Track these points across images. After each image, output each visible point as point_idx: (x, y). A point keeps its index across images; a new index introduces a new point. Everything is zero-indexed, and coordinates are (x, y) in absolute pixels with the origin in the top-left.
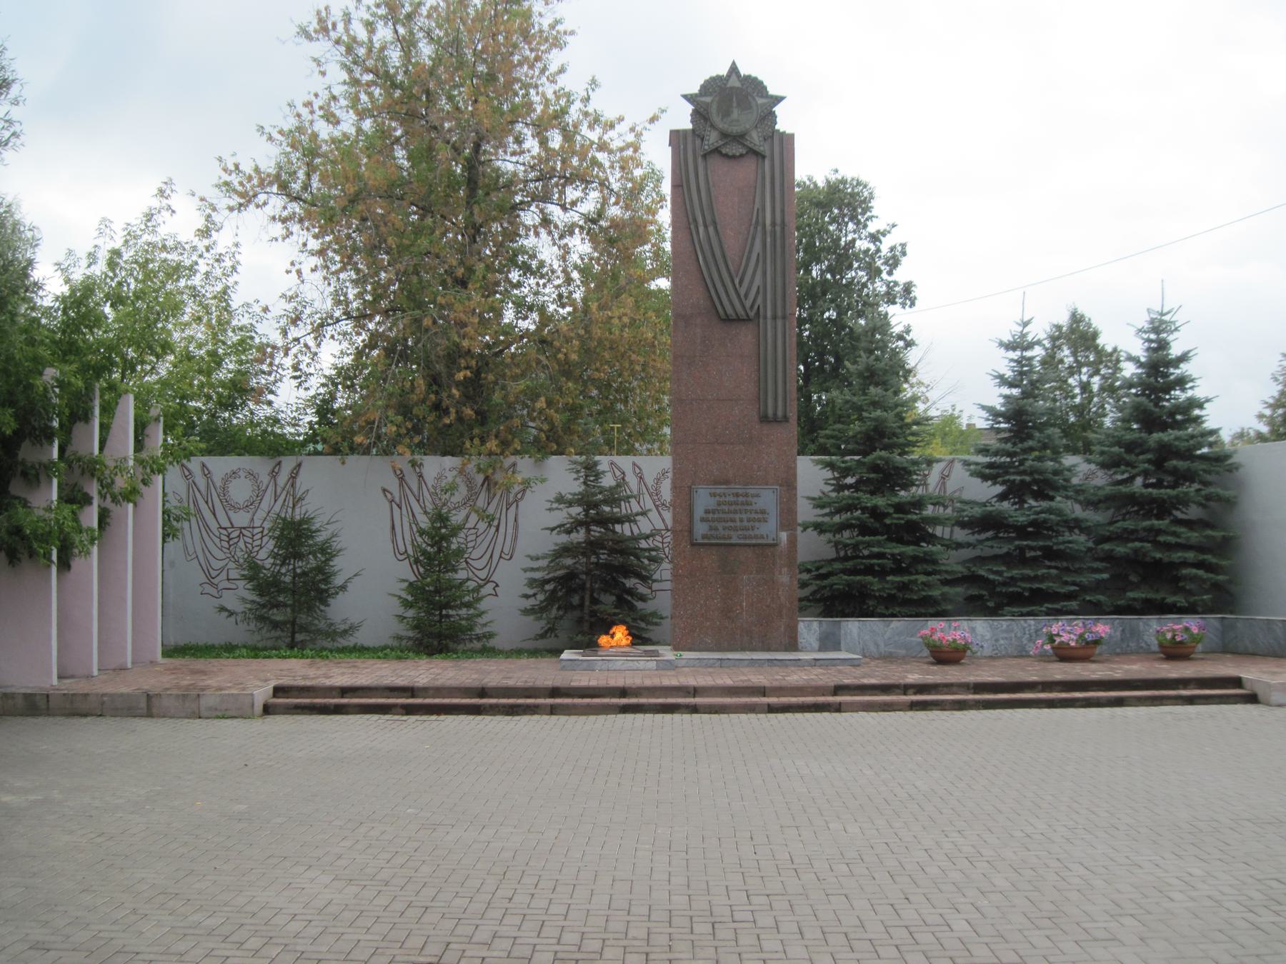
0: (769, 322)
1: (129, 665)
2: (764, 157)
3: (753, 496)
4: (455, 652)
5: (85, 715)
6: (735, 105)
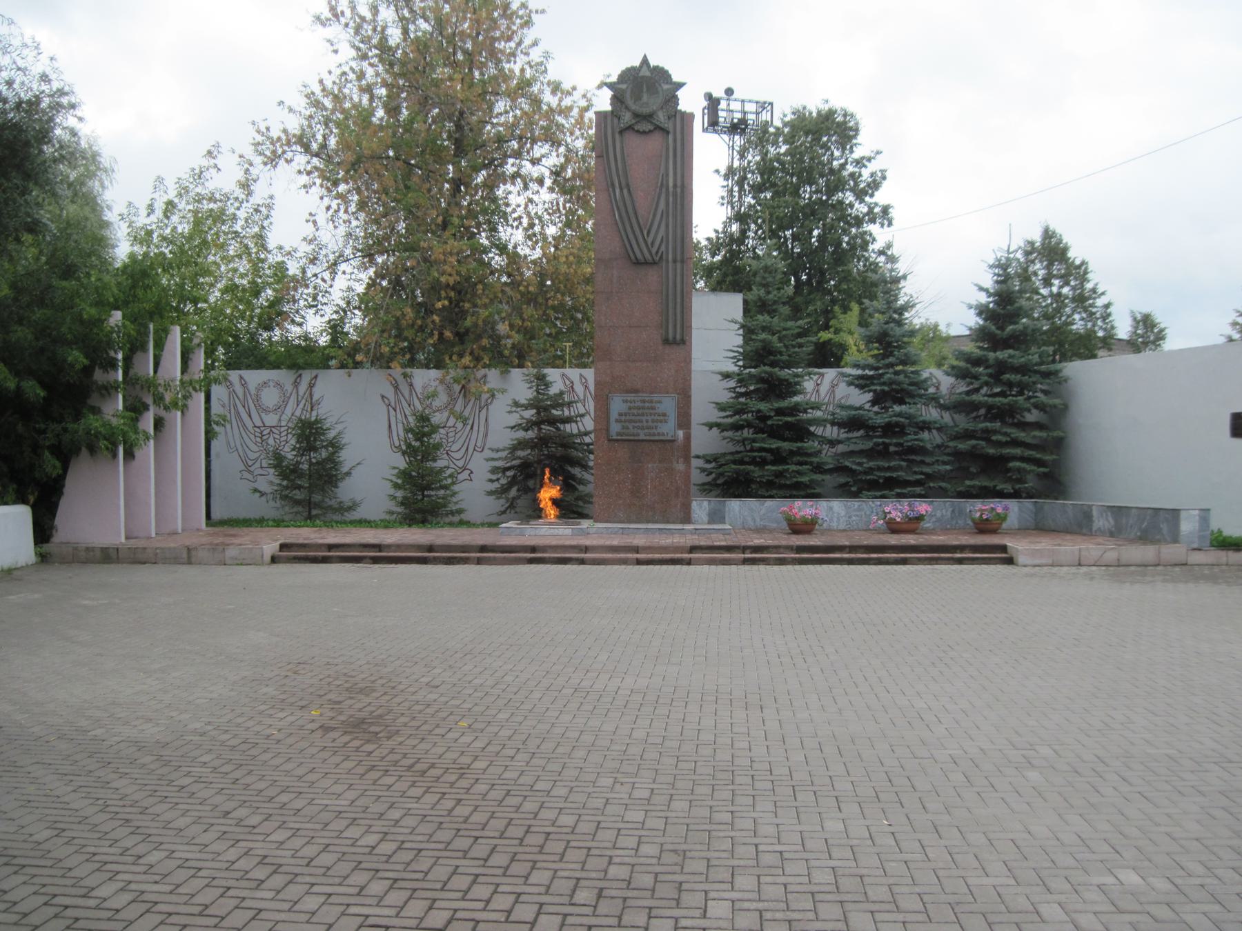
0: (670, 264)
1: (180, 531)
2: (668, 133)
3: (657, 402)
4: (431, 524)
5: (145, 563)
6: (645, 90)
